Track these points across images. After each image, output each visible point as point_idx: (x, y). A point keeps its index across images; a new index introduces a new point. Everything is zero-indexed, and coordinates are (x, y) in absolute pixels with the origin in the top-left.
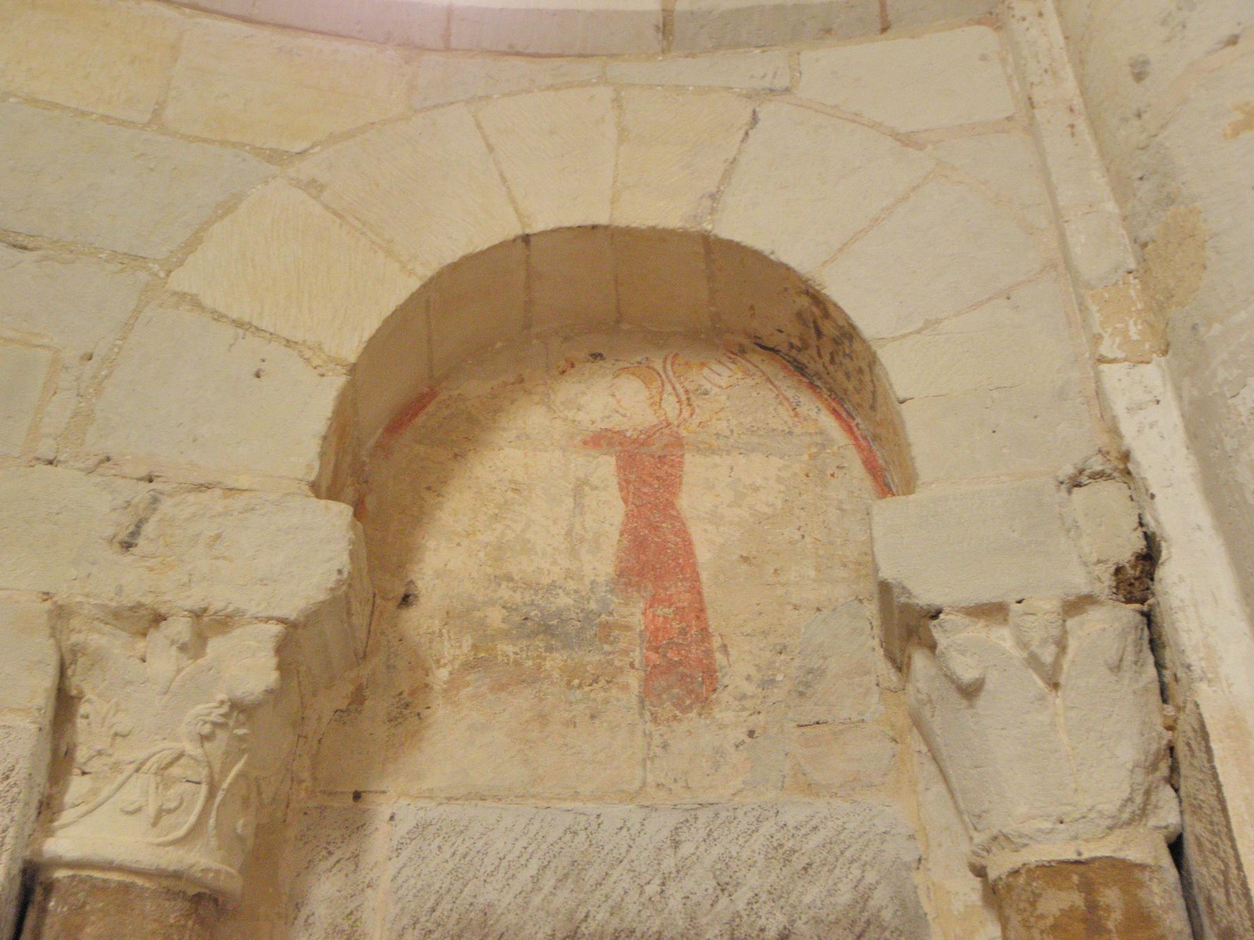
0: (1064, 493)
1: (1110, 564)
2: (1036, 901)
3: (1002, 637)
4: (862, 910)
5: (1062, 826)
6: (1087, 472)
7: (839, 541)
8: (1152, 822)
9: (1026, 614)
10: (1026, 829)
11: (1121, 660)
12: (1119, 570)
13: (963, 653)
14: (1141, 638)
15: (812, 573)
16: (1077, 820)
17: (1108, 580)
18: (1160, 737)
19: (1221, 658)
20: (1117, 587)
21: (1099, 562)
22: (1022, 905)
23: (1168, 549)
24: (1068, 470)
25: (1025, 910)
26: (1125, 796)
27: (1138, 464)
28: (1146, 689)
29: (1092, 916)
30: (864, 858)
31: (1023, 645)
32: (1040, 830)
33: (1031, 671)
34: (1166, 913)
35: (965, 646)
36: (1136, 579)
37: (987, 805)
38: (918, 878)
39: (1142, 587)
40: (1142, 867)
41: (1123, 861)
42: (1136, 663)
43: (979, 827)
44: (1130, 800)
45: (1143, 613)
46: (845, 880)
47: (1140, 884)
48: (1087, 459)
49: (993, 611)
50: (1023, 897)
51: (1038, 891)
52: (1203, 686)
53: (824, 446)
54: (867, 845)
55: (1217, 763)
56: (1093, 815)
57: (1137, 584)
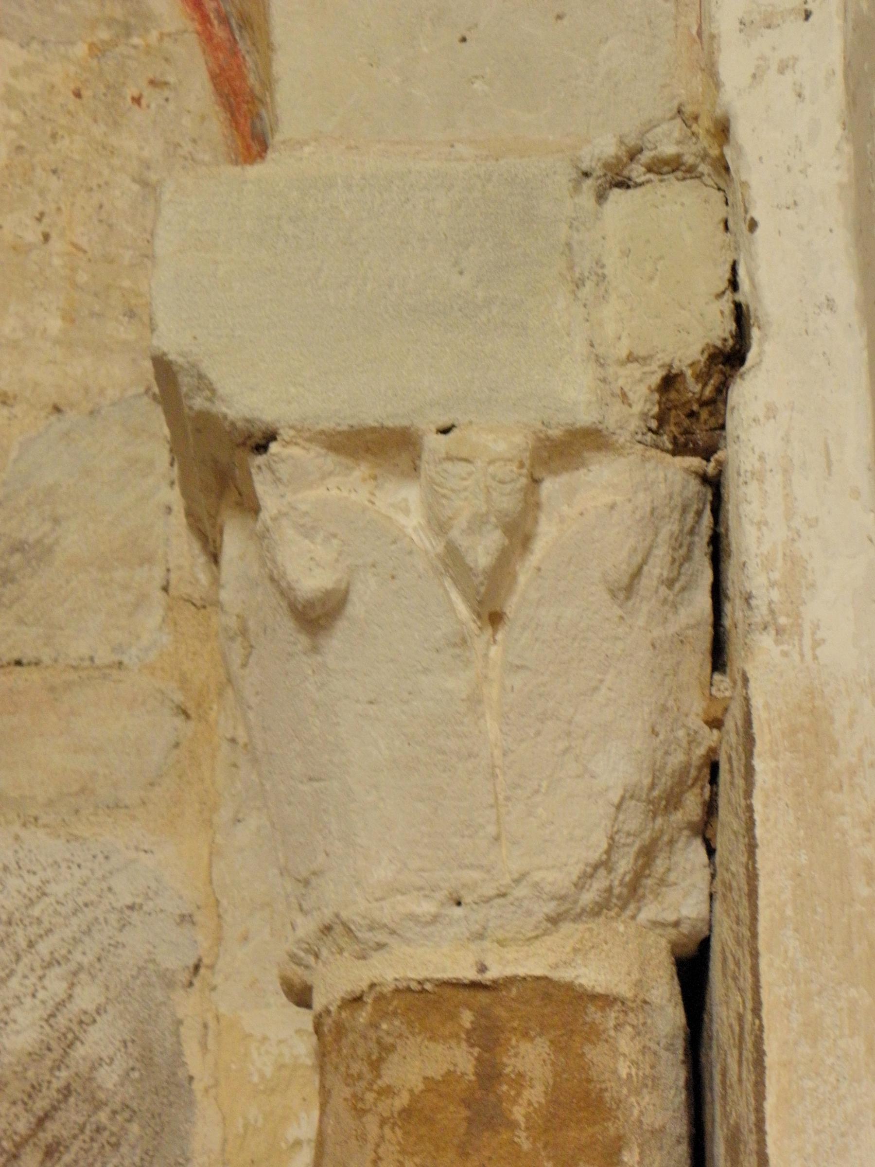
0: (587, 199)
1: (654, 367)
2: (381, 1060)
3: (402, 505)
4: (57, 1066)
5: (458, 911)
6: (646, 157)
7: (127, 256)
8: (649, 912)
9: (449, 458)
10: (386, 913)
11: (637, 574)
12: (669, 382)
13: (308, 531)
14: (692, 532)
15: (55, 325)
16: (488, 900)
17: (643, 400)
18: (693, 740)
19: (812, 586)
20: (662, 419)
21: (631, 358)
22: (356, 1067)
23: (761, 344)
24: (606, 146)
25: (360, 1077)
26: (596, 855)
27: (739, 150)
28: (681, 640)
29: (483, 1099)
30: (77, 956)
31: (439, 526)
32: (413, 917)
33: (448, 583)
34: (638, 1093)
35: (313, 518)
36: (703, 404)
37: (321, 858)
38: (187, 1005)
39: (712, 422)
40: (606, 1001)
41: (569, 987)
42: (670, 583)
43: (305, 907)
44: (605, 864)
45: (705, 479)
46: (28, 1001)
47: (594, 1034)
48: (652, 125)
49: (385, 447)
50: (360, 1051)
51: (389, 1040)
52: (765, 641)
53: (128, 30)
54: (88, 932)
55: (757, 802)
56: (521, 891)
57: (704, 414)
